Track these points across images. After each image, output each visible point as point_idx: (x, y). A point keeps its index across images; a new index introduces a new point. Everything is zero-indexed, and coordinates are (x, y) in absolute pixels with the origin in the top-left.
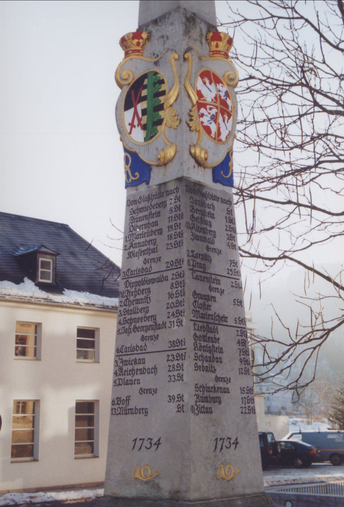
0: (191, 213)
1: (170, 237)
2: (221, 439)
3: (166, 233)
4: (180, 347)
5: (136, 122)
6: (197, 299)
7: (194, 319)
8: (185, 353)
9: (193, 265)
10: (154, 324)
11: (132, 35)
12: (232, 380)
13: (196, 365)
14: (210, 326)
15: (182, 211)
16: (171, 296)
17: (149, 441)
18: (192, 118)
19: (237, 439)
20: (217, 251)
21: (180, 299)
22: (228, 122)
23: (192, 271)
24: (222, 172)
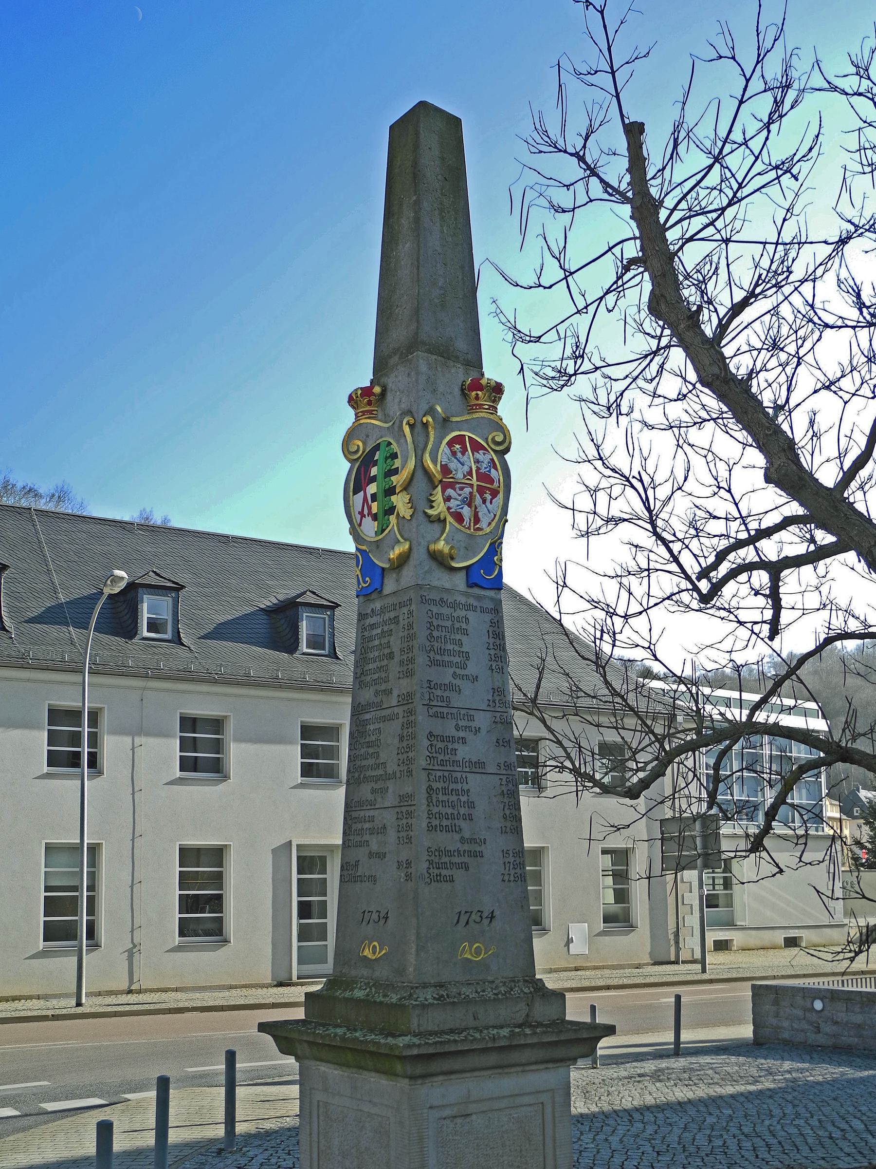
0: (429, 631)
1: (401, 663)
2: (369, 912)
3: (397, 658)
4: (410, 803)
5: (366, 512)
6: (435, 742)
7: (427, 767)
8: (415, 810)
9: (430, 699)
10: (383, 773)
11: (359, 392)
12: (488, 842)
13: (429, 825)
14: (454, 775)
15: (415, 630)
16: (401, 738)
17: (378, 914)
18: (434, 504)
19: (493, 912)
20: (471, 678)
21: (411, 742)
22: (491, 503)
23: (427, 707)
24: (482, 571)
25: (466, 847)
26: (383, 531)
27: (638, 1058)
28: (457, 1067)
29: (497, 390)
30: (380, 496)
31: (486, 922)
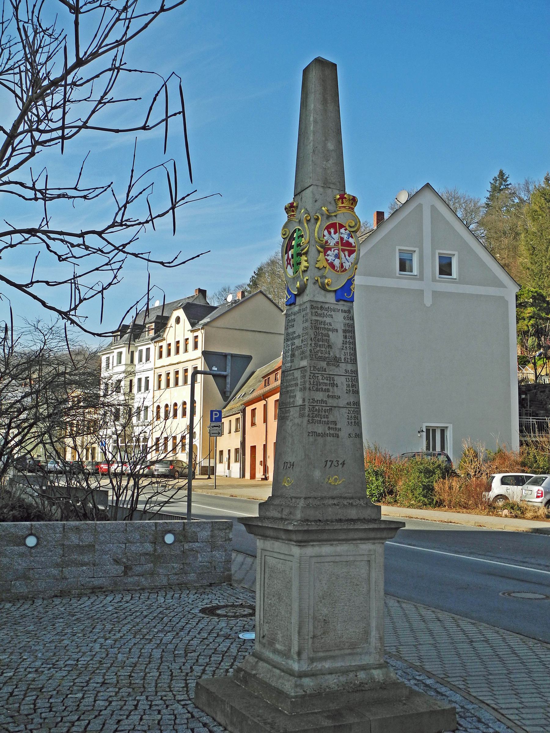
3: (299, 386)
12: (342, 430)
25: (332, 432)
26: (296, 272)
27: (454, 677)
28: (312, 98)
29: (354, 200)
30: (295, 256)
31: (340, 466)
